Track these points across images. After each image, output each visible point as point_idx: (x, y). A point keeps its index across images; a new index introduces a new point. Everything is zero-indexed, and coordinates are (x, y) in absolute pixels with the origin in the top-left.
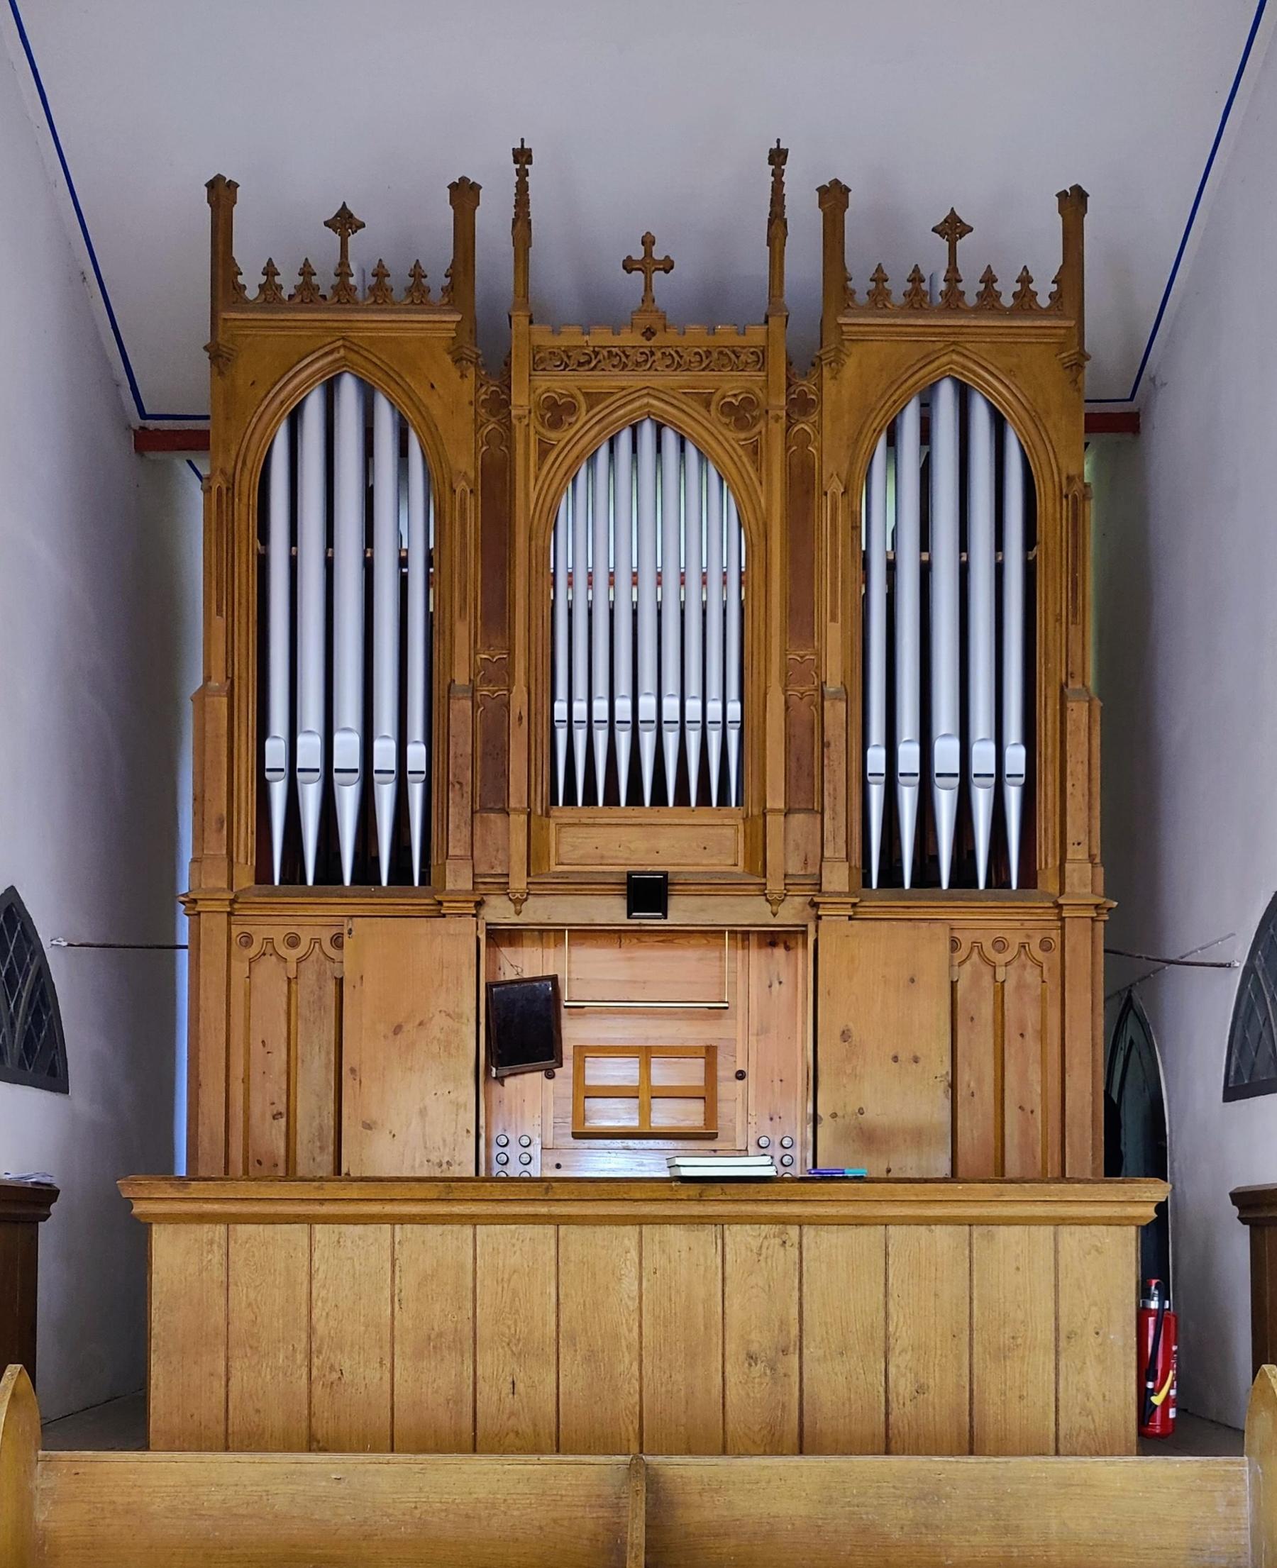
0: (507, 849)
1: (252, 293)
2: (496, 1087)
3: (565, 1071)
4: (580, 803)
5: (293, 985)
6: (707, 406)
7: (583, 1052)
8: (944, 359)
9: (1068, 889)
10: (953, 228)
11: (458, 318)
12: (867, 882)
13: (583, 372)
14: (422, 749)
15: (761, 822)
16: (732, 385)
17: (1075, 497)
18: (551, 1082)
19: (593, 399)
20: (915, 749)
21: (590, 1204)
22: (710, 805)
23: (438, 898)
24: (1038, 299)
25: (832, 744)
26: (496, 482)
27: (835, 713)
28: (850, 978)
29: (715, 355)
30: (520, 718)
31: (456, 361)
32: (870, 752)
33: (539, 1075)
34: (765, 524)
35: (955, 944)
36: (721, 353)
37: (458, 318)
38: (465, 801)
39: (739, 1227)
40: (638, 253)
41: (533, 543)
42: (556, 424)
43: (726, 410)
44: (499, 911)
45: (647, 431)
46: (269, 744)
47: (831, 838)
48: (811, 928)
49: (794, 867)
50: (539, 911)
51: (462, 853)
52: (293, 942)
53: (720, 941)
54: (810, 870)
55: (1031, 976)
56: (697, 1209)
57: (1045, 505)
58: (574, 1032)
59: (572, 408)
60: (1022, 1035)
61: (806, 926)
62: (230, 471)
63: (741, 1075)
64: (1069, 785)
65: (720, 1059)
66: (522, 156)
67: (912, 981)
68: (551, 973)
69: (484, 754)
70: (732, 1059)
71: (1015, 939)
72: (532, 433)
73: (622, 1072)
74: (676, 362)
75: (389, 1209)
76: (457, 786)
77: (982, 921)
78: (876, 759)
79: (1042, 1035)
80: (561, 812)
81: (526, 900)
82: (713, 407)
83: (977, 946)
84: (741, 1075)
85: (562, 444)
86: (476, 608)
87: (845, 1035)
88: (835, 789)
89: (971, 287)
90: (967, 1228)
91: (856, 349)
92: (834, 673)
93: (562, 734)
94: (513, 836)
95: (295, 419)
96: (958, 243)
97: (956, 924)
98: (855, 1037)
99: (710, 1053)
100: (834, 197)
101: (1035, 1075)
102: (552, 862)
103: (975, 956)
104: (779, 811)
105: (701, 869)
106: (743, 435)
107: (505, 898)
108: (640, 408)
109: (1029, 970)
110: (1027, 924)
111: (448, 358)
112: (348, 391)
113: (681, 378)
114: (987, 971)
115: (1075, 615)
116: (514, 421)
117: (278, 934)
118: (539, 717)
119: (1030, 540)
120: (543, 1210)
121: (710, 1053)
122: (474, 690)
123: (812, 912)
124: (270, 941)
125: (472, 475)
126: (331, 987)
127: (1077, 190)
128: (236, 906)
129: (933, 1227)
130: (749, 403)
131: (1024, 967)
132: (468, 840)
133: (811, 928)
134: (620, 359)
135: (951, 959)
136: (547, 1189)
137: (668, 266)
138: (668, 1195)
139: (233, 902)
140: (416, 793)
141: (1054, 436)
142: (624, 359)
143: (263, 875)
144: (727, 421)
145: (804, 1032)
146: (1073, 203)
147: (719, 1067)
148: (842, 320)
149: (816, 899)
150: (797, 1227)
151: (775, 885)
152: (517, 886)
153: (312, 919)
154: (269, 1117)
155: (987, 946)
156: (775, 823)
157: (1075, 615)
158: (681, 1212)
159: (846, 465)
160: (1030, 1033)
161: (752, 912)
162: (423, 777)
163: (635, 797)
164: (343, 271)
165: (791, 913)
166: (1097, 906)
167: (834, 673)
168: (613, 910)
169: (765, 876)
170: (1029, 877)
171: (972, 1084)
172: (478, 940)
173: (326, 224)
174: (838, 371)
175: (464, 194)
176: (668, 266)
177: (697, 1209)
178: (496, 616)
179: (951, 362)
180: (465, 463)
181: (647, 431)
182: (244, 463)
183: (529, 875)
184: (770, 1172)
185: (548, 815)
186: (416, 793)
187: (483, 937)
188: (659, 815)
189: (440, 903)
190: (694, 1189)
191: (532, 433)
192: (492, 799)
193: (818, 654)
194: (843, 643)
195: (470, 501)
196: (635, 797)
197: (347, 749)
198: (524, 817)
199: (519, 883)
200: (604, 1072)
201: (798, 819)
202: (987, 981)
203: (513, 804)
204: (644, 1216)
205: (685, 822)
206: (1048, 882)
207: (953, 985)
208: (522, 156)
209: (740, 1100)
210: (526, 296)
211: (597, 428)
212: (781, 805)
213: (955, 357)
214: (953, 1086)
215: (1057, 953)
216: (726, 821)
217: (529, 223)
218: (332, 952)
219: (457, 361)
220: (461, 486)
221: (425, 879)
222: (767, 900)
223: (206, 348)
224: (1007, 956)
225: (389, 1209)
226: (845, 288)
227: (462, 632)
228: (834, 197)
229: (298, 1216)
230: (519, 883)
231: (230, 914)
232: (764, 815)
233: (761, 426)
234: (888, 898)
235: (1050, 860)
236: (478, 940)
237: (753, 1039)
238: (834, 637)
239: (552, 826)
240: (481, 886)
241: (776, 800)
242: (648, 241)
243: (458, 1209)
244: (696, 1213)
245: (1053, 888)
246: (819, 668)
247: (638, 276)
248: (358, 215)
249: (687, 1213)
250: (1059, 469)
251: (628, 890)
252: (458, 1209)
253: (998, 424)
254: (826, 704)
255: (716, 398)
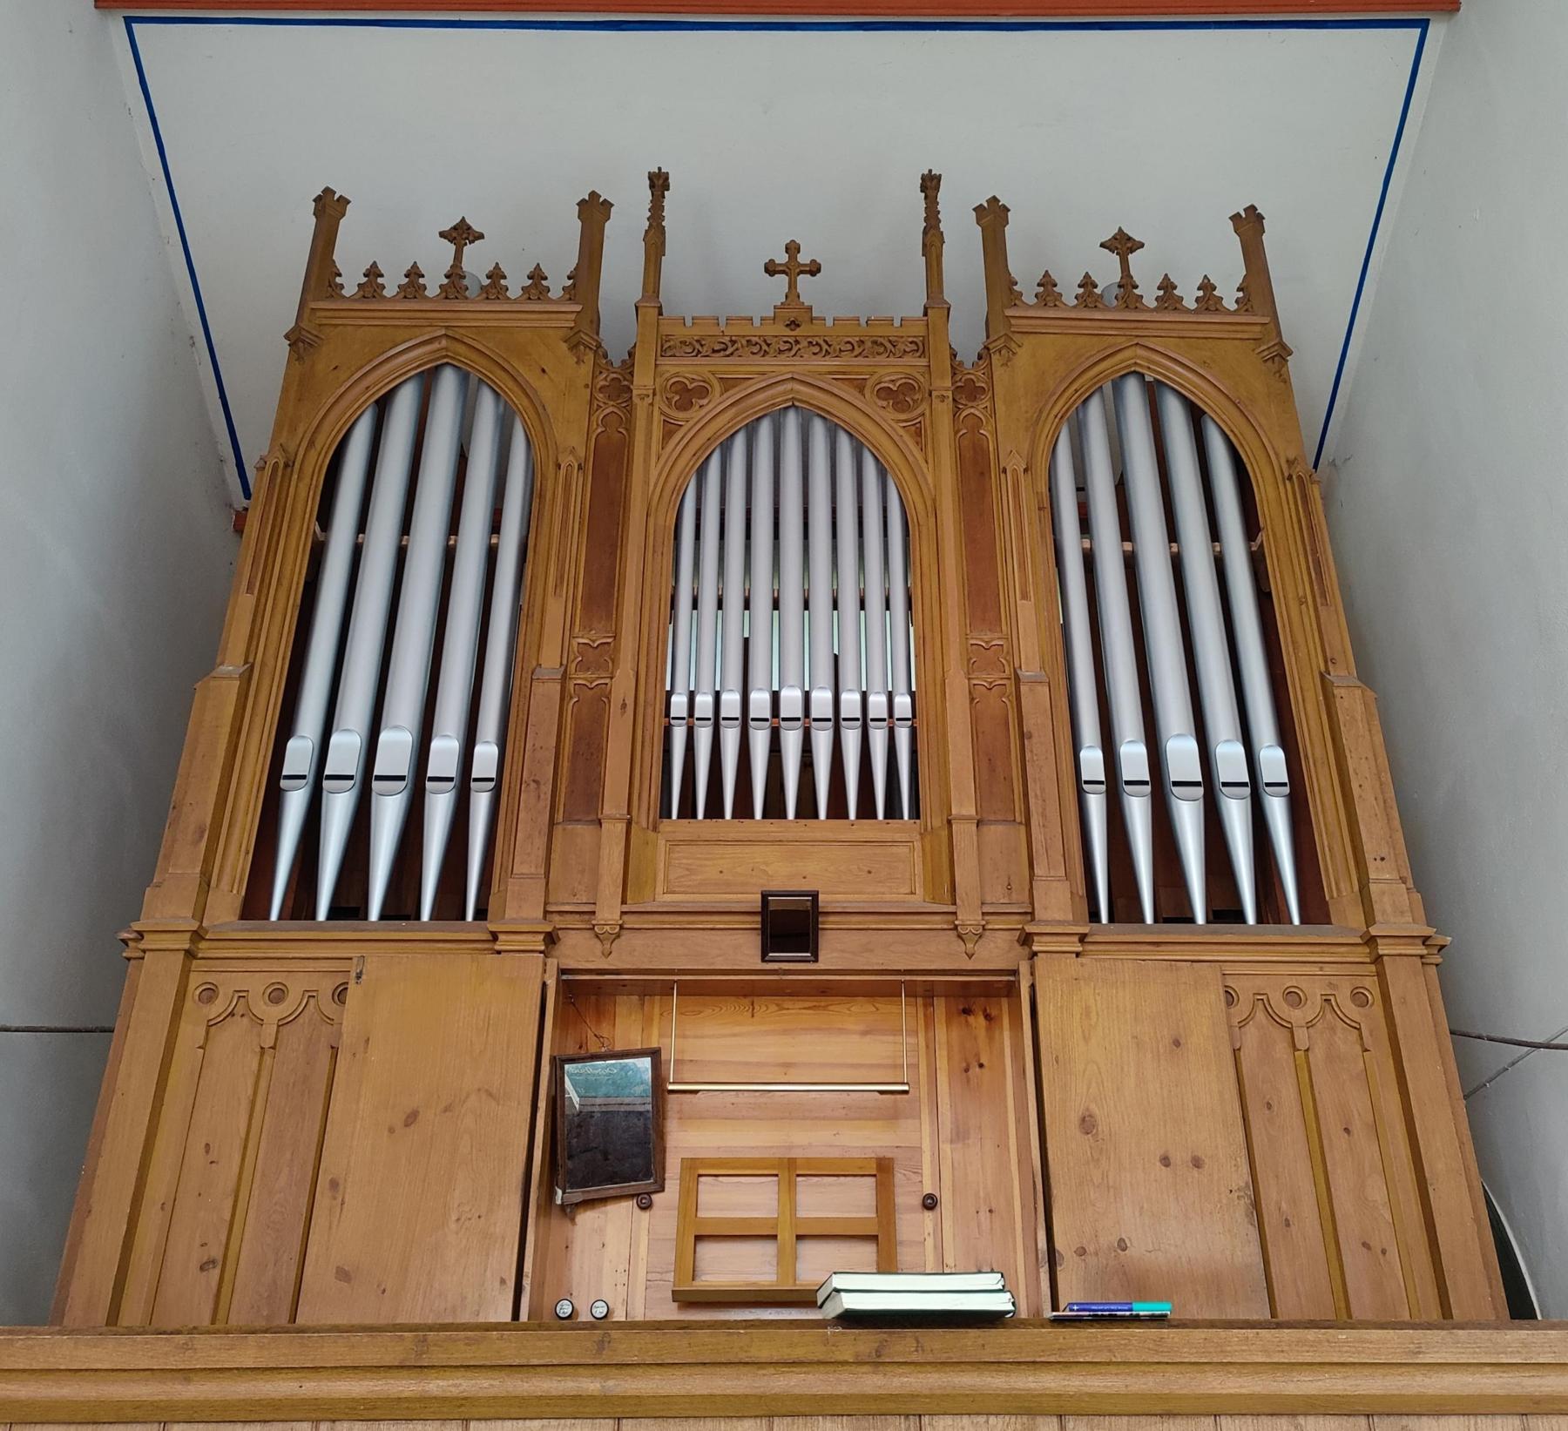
0: (595, 873)
1: (350, 290)
2: (556, 1221)
3: (669, 1198)
4: (700, 815)
5: (268, 1059)
6: (861, 390)
7: (695, 1169)
8: (1127, 354)
9: (1378, 917)
10: (1122, 245)
11: (578, 308)
12: (1094, 916)
13: (717, 359)
14: (494, 750)
15: (945, 833)
16: (890, 370)
17: (1299, 477)
18: (645, 1215)
19: (728, 384)
20: (1141, 750)
21: (678, 1372)
22: (875, 817)
23: (493, 928)
24: (1224, 303)
25: (1035, 734)
26: (610, 465)
27: (1036, 701)
28: (1086, 1039)
29: (868, 344)
30: (624, 706)
31: (571, 349)
32: (1083, 754)
33: (628, 1206)
34: (934, 501)
35: (1230, 997)
36: (875, 343)
37: (578, 308)
38: (542, 804)
39: (949, 1420)
40: (782, 258)
41: (651, 520)
42: (684, 406)
43: (883, 394)
44: (580, 952)
45: (792, 423)
46: (292, 744)
47: (1042, 851)
48: (1024, 969)
49: (997, 896)
50: (639, 953)
51: (533, 870)
52: (277, 995)
53: (894, 1009)
54: (1014, 897)
55: (1345, 1042)
56: (871, 1382)
57: (1265, 492)
58: (684, 1140)
59: (703, 392)
60: (1347, 1130)
61: (1015, 972)
62: (292, 448)
63: (930, 1203)
64: (1355, 785)
65: (899, 1177)
66: (659, 183)
67: (1177, 1043)
68: (655, 1045)
69: (575, 754)
70: (916, 1178)
71: (1315, 991)
72: (656, 413)
73: (752, 1200)
74: (823, 347)
75: (312, 1388)
76: (533, 785)
77: (1268, 963)
78: (1092, 760)
79: (1376, 1128)
80: (674, 825)
81: (618, 936)
82: (867, 392)
83: (1262, 1000)
84: (930, 1203)
85: (691, 423)
86: (576, 586)
87: (1087, 1124)
88: (1043, 790)
89: (1149, 293)
90: (1363, 1421)
91: (1028, 342)
92: (1031, 655)
93: (679, 735)
94: (605, 852)
95: (383, 406)
96: (1130, 256)
97: (1228, 969)
98: (1102, 1127)
99: (883, 1170)
100: (993, 216)
101: (1377, 1192)
102: (659, 889)
103: (1260, 1015)
104: (968, 818)
105: (864, 897)
106: (903, 417)
107: (588, 934)
108: (785, 393)
109: (1339, 1033)
110: (1328, 970)
111: (564, 346)
112: (448, 385)
113: (831, 363)
114: (1280, 1036)
115: (1323, 596)
116: (636, 400)
117: (257, 986)
118: (650, 710)
119: (1251, 526)
120: (591, 1385)
121: (883, 1170)
122: (565, 678)
123: (1026, 951)
124: (242, 995)
125: (581, 453)
126: (325, 1055)
127: (1251, 209)
128: (203, 945)
129: (1301, 1420)
130: (908, 388)
131: (1333, 1029)
132: (542, 853)
133: (1024, 969)
134: (762, 347)
135: (1229, 1016)
136: (601, 1346)
137: (814, 269)
138: (819, 1353)
139: (197, 936)
140: (481, 803)
141: (1263, 421)
142: (765, 347)
143: (254, 906)
144: (884, 403)
145: (1021, 1120)
146: (1249, 224)
147: (898, 1190)
148: (1009, 313)
149: (1029, 929)
150: (1055, 1419)
151: (969, 917)
152: (607, 916)
153: (310, 956)
154: (194, 1266)
155: (1276, 999)
156: (964, 834)
157: (1323, 596)
158: (843, 1389)
159: (1026, 446)
160: (1357, 1127)
161: (935, 953)
162: (492, 784)
163: (775, 808)
164: (455, 274)
165: (995, 953)
166: (1425, 940)
167: (1031, 655)
168: (740, 950)
169: (954, 903)
170: (1315, 909)
171: (1284, 1205)
172: (544, 985)
173: (442, 235)
174: (1009, 360)
175: (594, 211)
176: (814, 269)
177: (871, 1382)
178: (601, 596)
179: (1136, 357)
180: (573, 435)
181: (792, 423)
182: (311, 443)
183: (624, 902)
184: (1001, 1303)
185: (655, 829)
186: (481, 803)
187: (552, 983)
188: (807, 828)
189: (494, 937)
190: (866, 1340)
191: (656, 413)
192: (579, 796)
193: (1009, 639)
194: (1038, 625)
195: (577, 479)
196: (775, 808)
197: (396, 745)
198: (621, 827)
199: (609, 913)
200: (725, 1200)
201: (994, 832)
202: (1281, 1049)
203: (608, 809)
204: (775, 1398)
205: (843, 837)
206: (1346, 914)
207: (1236, 1052)
208: (659, 183)
209: (930, 1243)
210: (657, 292)
211: (733, 411)
212: (971, 810)
213: (1140, 352)
214: (1256, 1204)
215: (1377, 1010)
216: (897, 837)
217: (663, 232)
218: (329, 1008)
219: (573, 348)
220: (566, 460)
221: (481, 914)
222: (959, 936)
223: (287, 337)
224: (1310, 1011)
225: (312, 1388)
226: (1011, 290)
227: (555, 611)
228: (993, 216)
229: (138, 1405)
230: (609, 913)
231: (190, 955)
232: (949, 822)
233: (924, 407)
234: (1125, 932)
235: (1342, 885)
236: (544, 985)
237: (946, 1148)
238: (1027, 617)
239: (662, 843)
240: (557, 918)
241: (964, 807)
242: (792, 249)
243: (436, 1386)
244: (869, 1390)
245: (1356, 919)
246: (1011, 651)
247: (782, 280)
248: (476, 228)
249: (855, 1391)
250: (1277, 454)
251: (763, 922)
252: (436, 1386)
253: (1196, 416)
254: (1023, 689)
255: (869, 384)
